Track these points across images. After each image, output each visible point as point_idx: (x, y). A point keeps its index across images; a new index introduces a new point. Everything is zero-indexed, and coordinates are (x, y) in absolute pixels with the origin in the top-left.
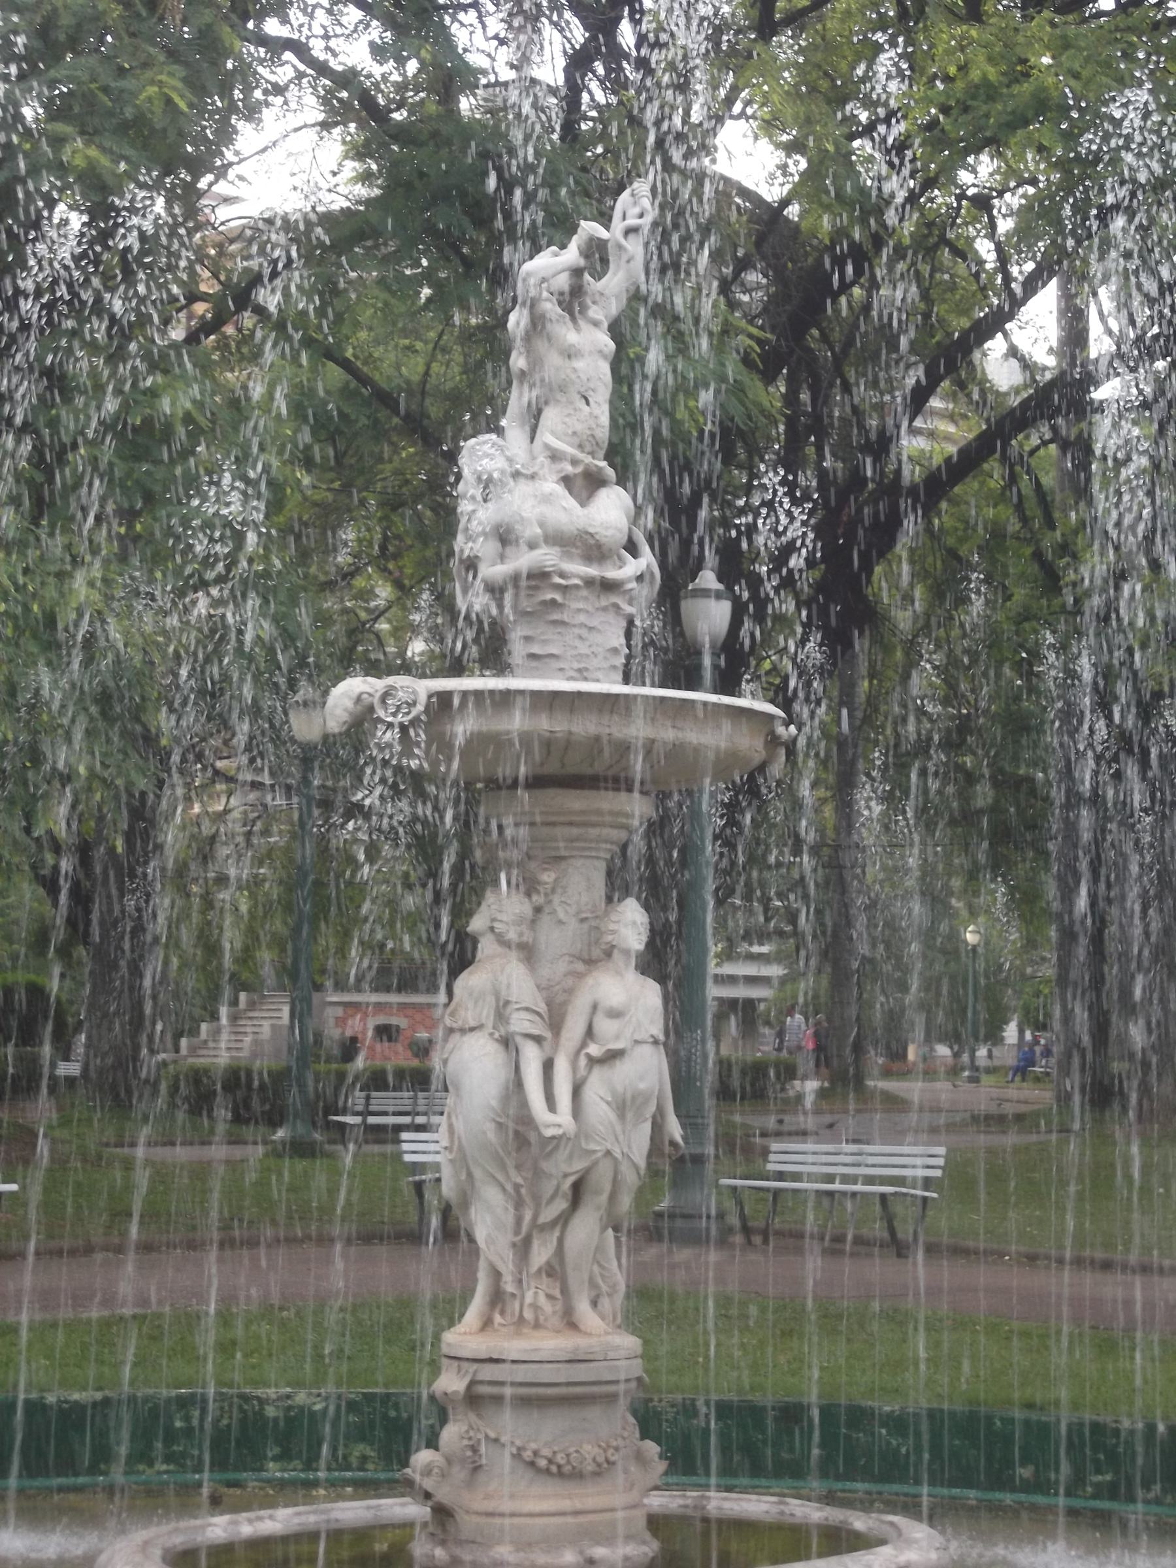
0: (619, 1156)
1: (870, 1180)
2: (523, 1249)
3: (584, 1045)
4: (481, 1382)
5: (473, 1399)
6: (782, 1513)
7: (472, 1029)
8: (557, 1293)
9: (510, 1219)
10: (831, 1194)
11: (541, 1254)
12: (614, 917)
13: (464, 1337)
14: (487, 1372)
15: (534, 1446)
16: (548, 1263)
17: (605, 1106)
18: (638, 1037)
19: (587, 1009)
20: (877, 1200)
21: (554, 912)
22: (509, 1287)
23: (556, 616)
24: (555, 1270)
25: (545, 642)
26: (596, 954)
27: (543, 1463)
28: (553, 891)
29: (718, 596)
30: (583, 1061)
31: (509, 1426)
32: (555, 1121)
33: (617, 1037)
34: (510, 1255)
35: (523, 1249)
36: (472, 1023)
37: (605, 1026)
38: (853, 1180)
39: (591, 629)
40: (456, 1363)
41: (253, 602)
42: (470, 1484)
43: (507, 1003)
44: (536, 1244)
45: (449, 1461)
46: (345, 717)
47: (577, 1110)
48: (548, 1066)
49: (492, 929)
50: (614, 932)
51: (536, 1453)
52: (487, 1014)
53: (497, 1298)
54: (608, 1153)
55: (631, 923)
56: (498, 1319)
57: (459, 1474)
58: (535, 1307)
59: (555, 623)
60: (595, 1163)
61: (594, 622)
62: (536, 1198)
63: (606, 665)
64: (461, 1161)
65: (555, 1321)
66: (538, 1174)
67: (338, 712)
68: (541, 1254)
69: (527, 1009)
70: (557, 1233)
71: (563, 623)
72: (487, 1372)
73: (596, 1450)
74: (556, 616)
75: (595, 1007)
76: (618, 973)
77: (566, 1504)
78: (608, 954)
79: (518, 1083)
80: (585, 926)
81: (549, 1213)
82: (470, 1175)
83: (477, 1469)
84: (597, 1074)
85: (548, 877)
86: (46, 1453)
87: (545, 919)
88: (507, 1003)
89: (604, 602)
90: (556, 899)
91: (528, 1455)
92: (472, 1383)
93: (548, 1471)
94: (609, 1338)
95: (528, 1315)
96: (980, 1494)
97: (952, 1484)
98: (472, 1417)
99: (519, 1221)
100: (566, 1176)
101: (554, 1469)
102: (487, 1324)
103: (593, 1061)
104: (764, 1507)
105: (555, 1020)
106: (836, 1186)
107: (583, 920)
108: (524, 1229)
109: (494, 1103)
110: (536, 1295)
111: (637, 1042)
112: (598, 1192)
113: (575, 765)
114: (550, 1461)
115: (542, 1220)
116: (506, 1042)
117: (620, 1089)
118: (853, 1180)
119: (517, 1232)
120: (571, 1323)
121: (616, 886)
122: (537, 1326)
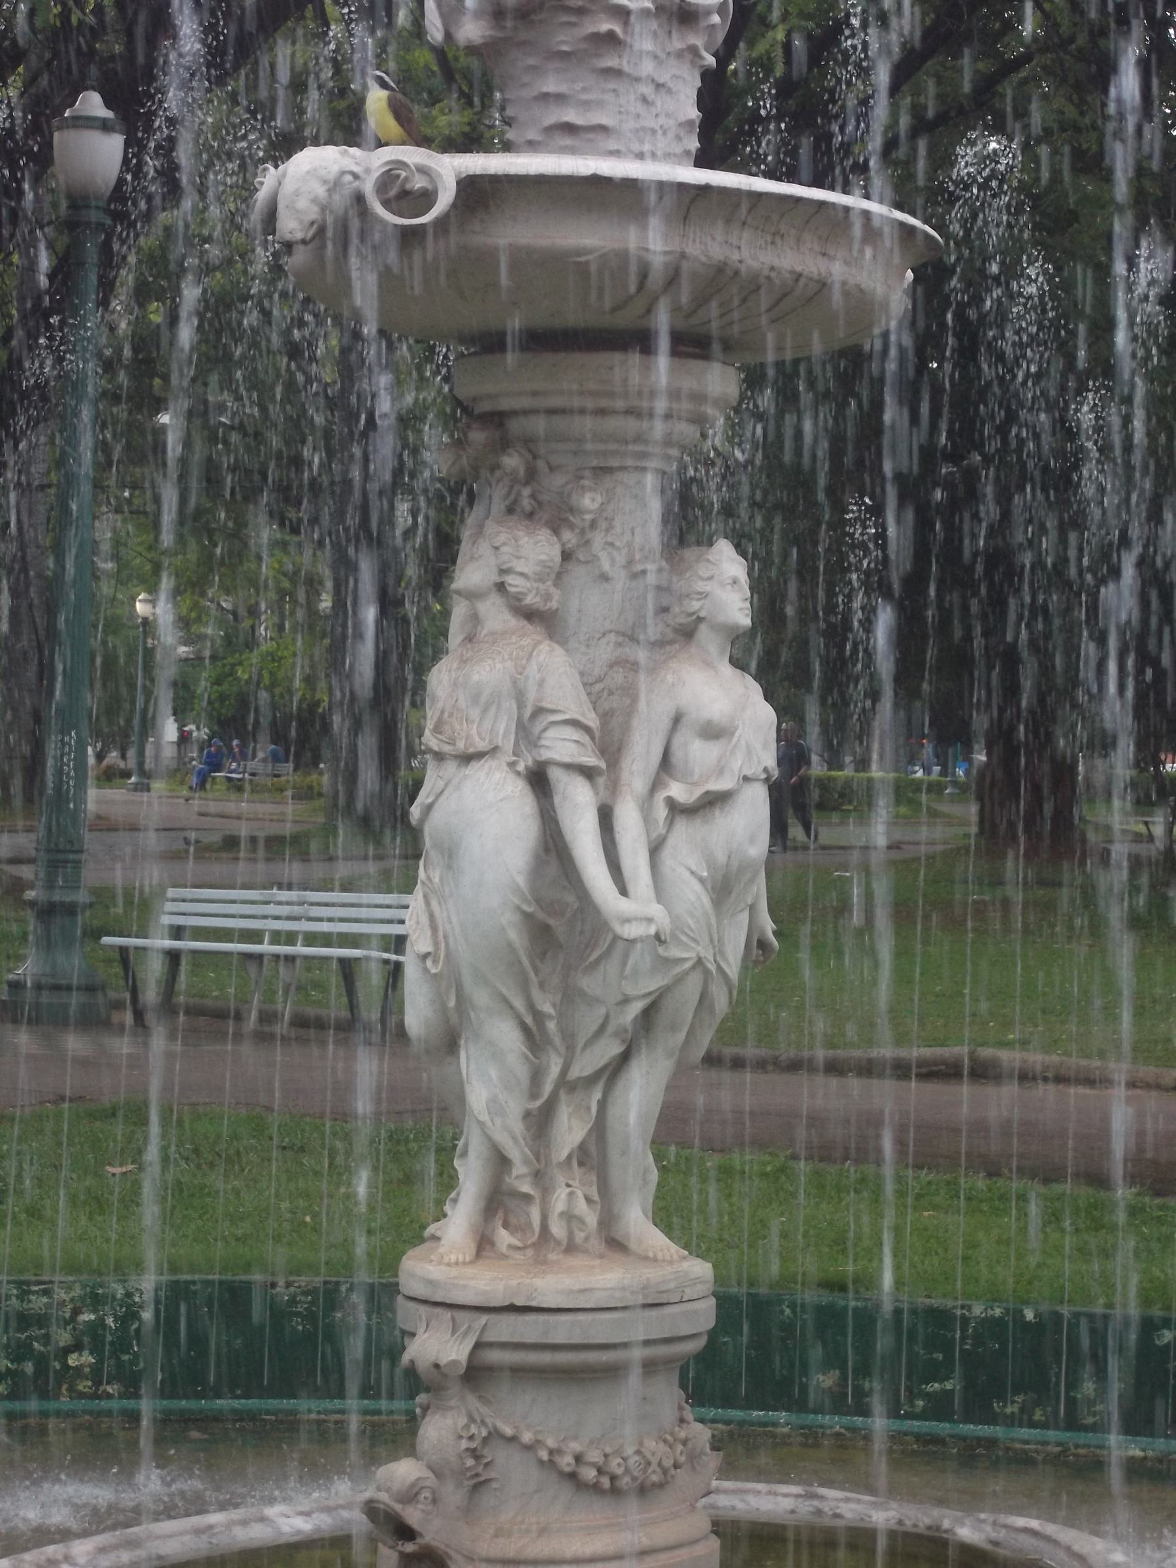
0: (712, 967)
2: (540, 1122)
4: (491, 1345)
5: (476, 1374)
6: (819, 1512)
7: (479, 756)
8: (594, 1193)
9: (522, 1072)
11: (570, 1131)
12: (703, 571)
13: (448, 1259)
14: (506, 1328)
15: (575, 1446)
16: (582, 1147)
17: (697, 886)
18: (749, 772)
19: (665, 723)
22: (520, 1180)
23: (610, 62)
24: (593, 1156)
25: (587, 105)
27: (590, 1474)
28: (593, 525)
29: (105, 126)
30: (661, 812)
31: (533, 1415)
32: (632, 910)
33: (720, 771)
34: (518, 1127)
35: (540, 1122)
36: (481, 745)
37: (697, 753)
38: (290, 938)
39: (659, 86)
40: (447, 1315)
41: (91, 20)
42: (469, 1511)
43: (539, 711)
45: (437, 1472)
46: (313, 213)
49: (501, 587)
50: (704, 595)
51: (578, 1459)
52: (502, 728)
53: (498, 1202)
54: (700, 962)
55: (724, 582)
56: (504, 1238)
57: (454, 1496)
58: (569, 1217)
60: (680, 980)
62: (569, 1037)
63: (678, 150)
64: (448, 981)
65: (596, 1244)
66: (570, 996)
68: (570, 1131)
70: (597, 1095)
71: (617, 73)
72: (506, 1328)
74: (610, 62)
75: (677, 720)
76: (708, 664)
79: (553, 846)
81: (585, 1066)
83: (479, 1486)
85: (589, 502)
86: (9, 1543)
87: (579, 573)
88: (539, 711)
89: (677, 44)
90: (598, 539)
91: (566, 1462)
92: (478, 1346)
93: (596, 1488)
94: (686, 1265)
95: (557, 1229)
96: (794, 1418)
97: (749, 1404)
98: (472, 1401)
99: (536, 1077)
100: (626, 1000)
101: (606, 1482)
102: (483, 1244)
103: (675, 809)
104: (787, 1504)
105: (611, 746)
108: (548, 1089)
109: (521, 880)
110: (570, 1197)
111: (746, 779)
112: (674, 1028)
113: (572, 315)
114: (600, 1471)
115: (575, 1073)
116: (539, 780)
117: (721, 857)
119: (534, 1095)
121: (687, 526)
122: (571, 1248)
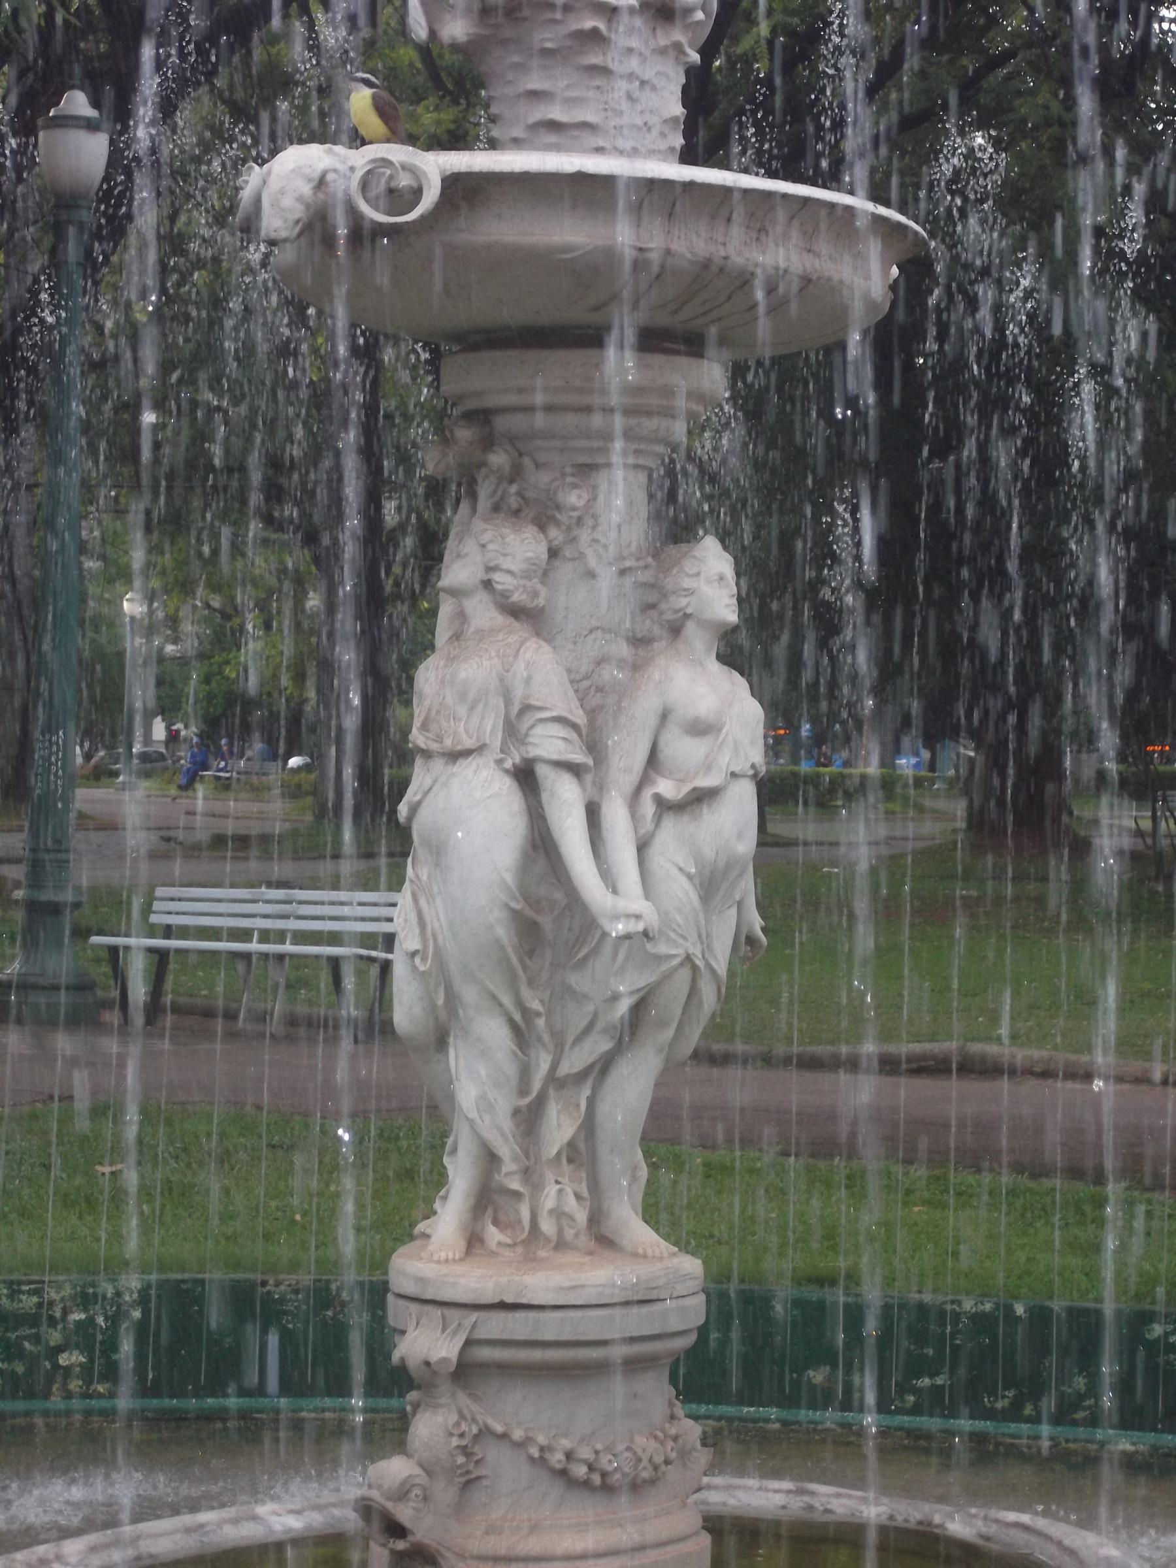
1: (302, 937)
2: (529, 1119)
3: (644, 781)
5: (465, 1372)
7: (467, 753)
9: (511, 1070)
10: (247, 956)
11: (559, 1128)
14: (495, 1326)
15: (566, 1443)
16: (571, 1145)
18: (737, 769)
19: (653, 721)
20: (324, 963)
21: (582, 556)
22: (510, 1178)
23: (595, 59)
26: (659, 625)
30: (648, 808)
31: (522, 1412)
33: (708, 767)
35: (529, 1119)
36: (469, 743)
37: (682, 750)
39: (643, 83)
40: (437, 1312)
42: (460, 1509)
44: (553, 1110)
47: (648, 889)
48: (593, 814)
49: (488, 584)
50: (689, 592)
51: (569, 1456)
52: (490, 726)
53: (487, 1199)
54: (688, 958)
55: (711, 580)
56: (494, 1235)
57: (445, 1493)
58: (558, 1214)
59: (593, 69)
61: (648, 74)
67: (287, 202)
68: (559, 1128)
69: (559, 720)
70: (586, 1092)
72: (495, 1326)
73: (653, 1444)
74: (594, 58)
75: (665, 716)
77: (627, 1536)
78: (675, 630)
80: (629, 581)
82: (452, 998)
83: (468, 1484)
84: (670, 824)
87: (565, 571)
88: (526, 708)
90: (584, 535)
91: (557, 1459)
92: (469, 1343)
94: (675, 1260)
95: (547, 1226)
98: (462, 1398)
99: (525, 1073)
101: (596, 1479)
102: (473, 1242)
103: (664, 806)
104: (779, 1499)
106: (254, 946)
107: (623, 572)
109: (509, 878)
110: (560, 1195)
111: (734, 775)
112: (662, 1024)
114: (591, 1468)
115: (564, 1069)
116: (526, 777)
117: (709, 853)
118: (280, 937)
119: (523, 1091)
120: (602, 1238)
122: (560, 1245)
